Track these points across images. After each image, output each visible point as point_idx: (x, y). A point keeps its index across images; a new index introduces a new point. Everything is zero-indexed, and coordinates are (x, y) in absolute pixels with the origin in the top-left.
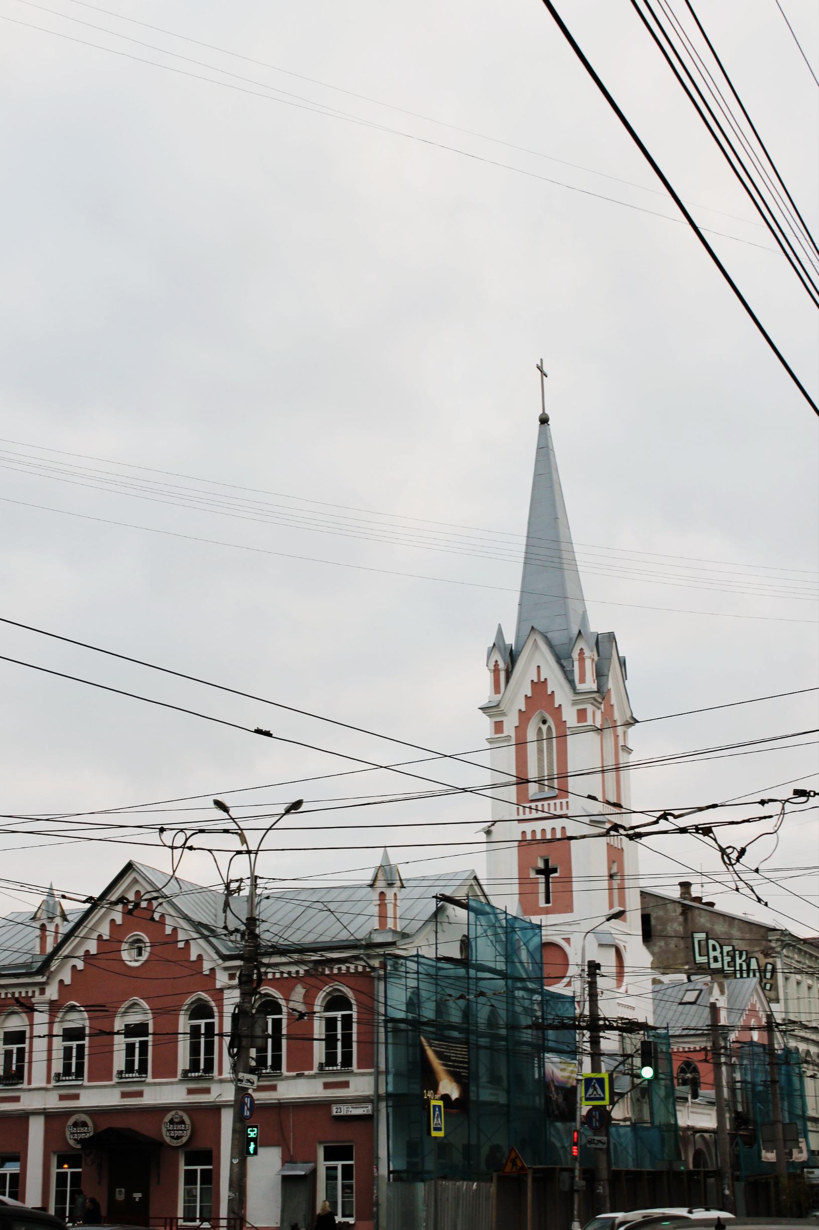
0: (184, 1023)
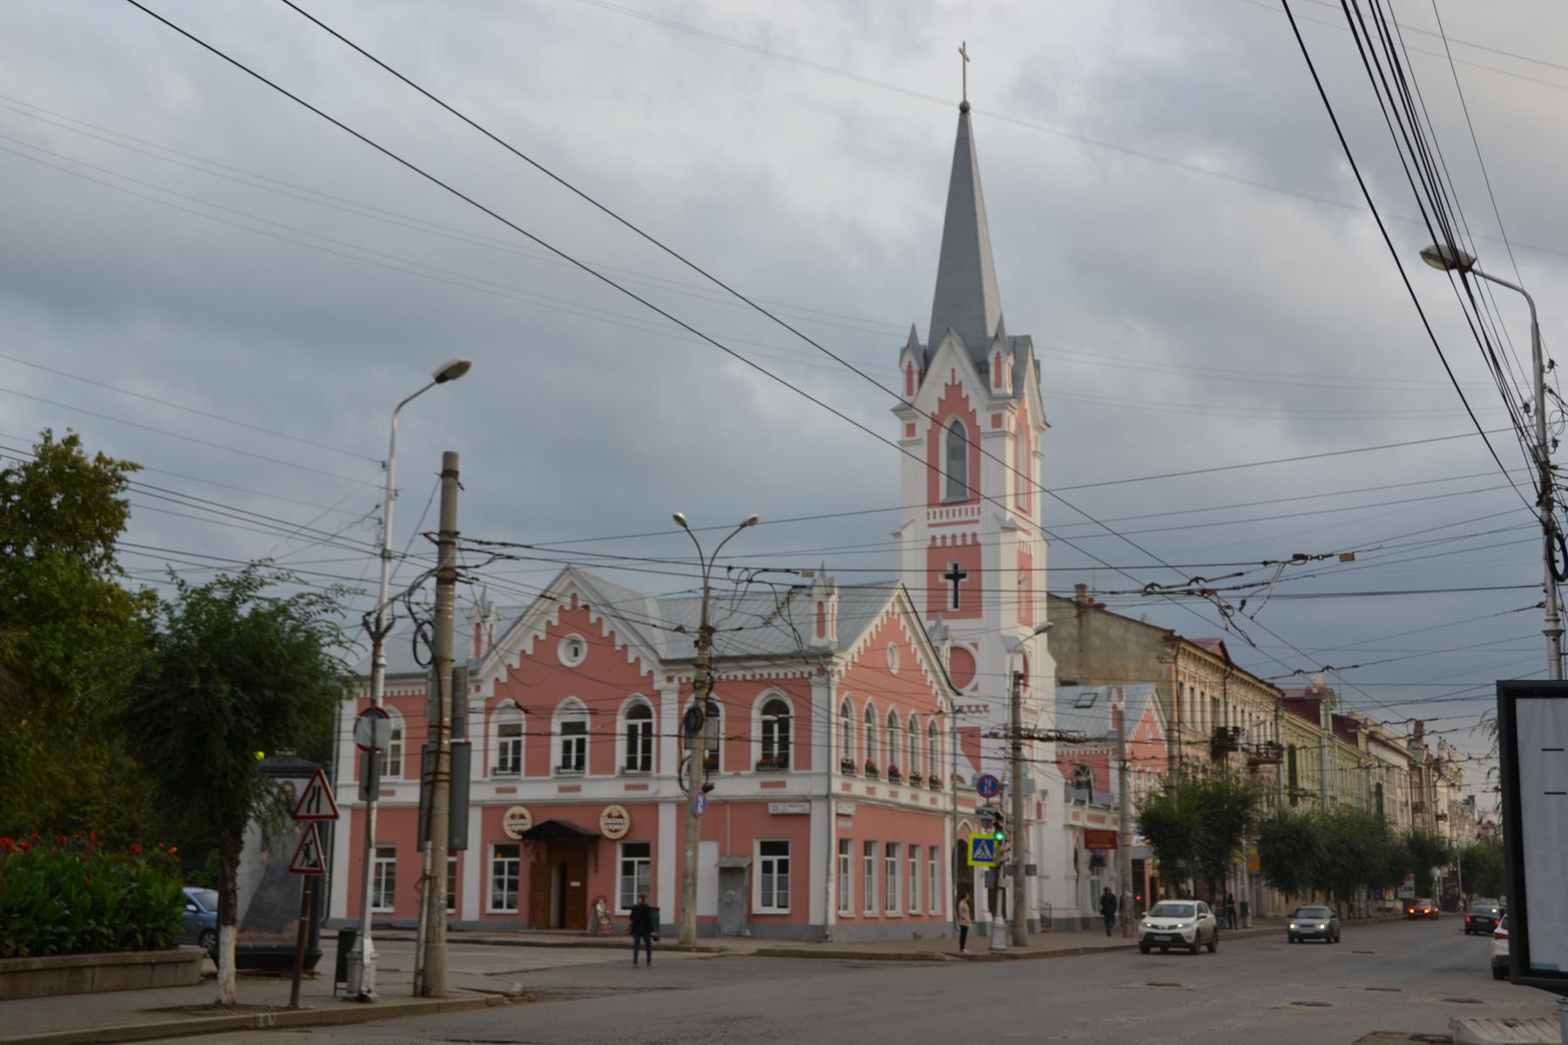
0: (621, 725)
